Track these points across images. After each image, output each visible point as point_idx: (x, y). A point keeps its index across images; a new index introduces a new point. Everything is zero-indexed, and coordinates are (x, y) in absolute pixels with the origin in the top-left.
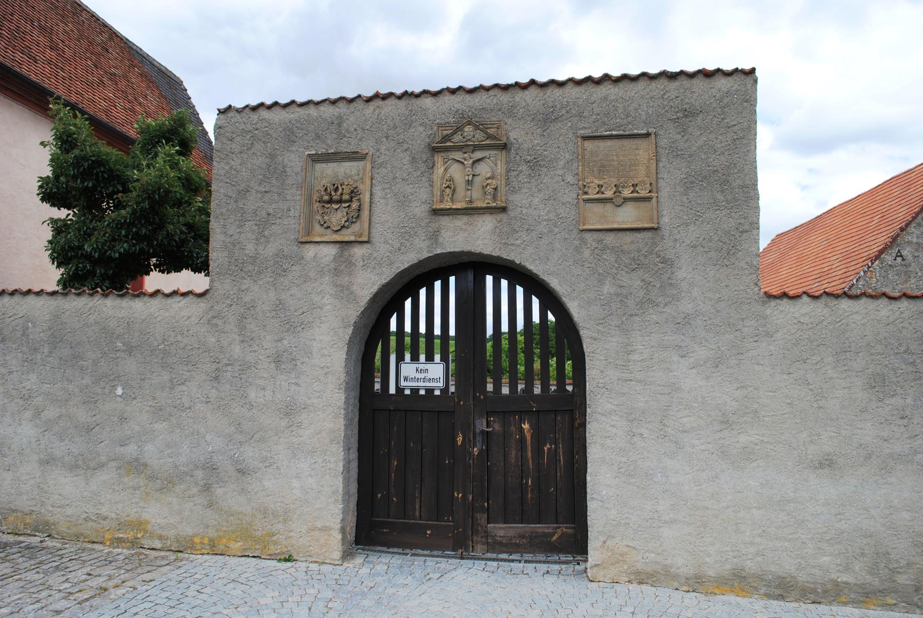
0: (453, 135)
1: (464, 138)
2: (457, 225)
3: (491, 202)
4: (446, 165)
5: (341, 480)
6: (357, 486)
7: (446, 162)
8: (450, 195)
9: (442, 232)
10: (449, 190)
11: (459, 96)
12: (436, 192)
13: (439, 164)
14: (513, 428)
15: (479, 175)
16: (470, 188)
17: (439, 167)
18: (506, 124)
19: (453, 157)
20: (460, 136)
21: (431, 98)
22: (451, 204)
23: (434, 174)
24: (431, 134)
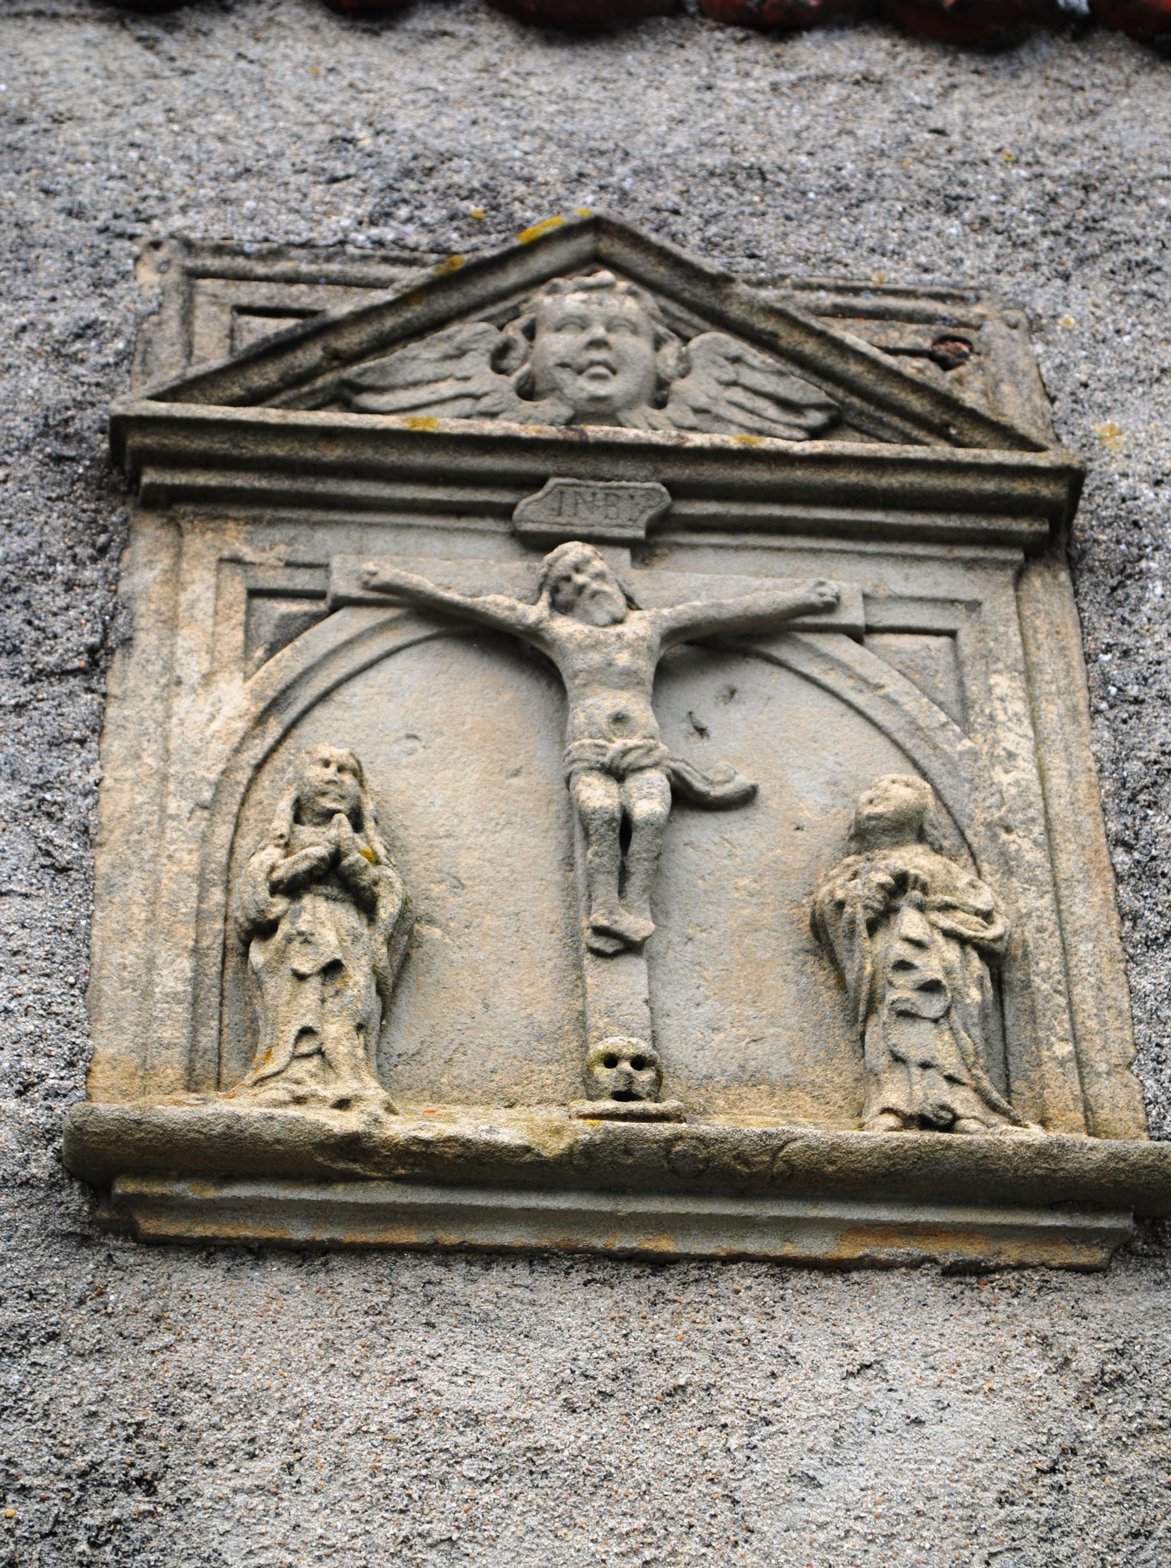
0: (383, 345)
1: (528, 391)
2: (457, 1396)
3: (962, 1101)
4: (289, 660)
5: (382, 911)
6: (819, 35)
7: (288, 633)
8: (359, 978)
9: (209, 1486)
10: (348, 917)
11: (436, 51)
12: (128, 954)
13: (189, 638)
14: (1003, 683)
15: (746, 799)
16: (636, 924)
17: (192, 668)
18: (1034, 326)
19: (389, 573)
20: (477, 366)
21: (92, 31)
22: (373, 1091)
23: (115, 745)
24: (87, 330)
